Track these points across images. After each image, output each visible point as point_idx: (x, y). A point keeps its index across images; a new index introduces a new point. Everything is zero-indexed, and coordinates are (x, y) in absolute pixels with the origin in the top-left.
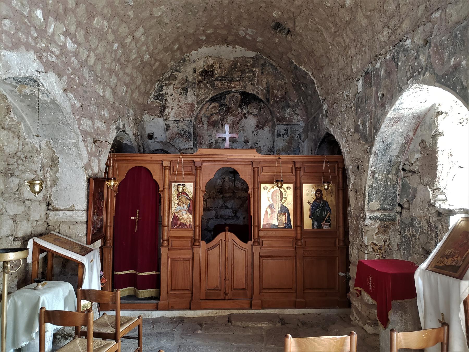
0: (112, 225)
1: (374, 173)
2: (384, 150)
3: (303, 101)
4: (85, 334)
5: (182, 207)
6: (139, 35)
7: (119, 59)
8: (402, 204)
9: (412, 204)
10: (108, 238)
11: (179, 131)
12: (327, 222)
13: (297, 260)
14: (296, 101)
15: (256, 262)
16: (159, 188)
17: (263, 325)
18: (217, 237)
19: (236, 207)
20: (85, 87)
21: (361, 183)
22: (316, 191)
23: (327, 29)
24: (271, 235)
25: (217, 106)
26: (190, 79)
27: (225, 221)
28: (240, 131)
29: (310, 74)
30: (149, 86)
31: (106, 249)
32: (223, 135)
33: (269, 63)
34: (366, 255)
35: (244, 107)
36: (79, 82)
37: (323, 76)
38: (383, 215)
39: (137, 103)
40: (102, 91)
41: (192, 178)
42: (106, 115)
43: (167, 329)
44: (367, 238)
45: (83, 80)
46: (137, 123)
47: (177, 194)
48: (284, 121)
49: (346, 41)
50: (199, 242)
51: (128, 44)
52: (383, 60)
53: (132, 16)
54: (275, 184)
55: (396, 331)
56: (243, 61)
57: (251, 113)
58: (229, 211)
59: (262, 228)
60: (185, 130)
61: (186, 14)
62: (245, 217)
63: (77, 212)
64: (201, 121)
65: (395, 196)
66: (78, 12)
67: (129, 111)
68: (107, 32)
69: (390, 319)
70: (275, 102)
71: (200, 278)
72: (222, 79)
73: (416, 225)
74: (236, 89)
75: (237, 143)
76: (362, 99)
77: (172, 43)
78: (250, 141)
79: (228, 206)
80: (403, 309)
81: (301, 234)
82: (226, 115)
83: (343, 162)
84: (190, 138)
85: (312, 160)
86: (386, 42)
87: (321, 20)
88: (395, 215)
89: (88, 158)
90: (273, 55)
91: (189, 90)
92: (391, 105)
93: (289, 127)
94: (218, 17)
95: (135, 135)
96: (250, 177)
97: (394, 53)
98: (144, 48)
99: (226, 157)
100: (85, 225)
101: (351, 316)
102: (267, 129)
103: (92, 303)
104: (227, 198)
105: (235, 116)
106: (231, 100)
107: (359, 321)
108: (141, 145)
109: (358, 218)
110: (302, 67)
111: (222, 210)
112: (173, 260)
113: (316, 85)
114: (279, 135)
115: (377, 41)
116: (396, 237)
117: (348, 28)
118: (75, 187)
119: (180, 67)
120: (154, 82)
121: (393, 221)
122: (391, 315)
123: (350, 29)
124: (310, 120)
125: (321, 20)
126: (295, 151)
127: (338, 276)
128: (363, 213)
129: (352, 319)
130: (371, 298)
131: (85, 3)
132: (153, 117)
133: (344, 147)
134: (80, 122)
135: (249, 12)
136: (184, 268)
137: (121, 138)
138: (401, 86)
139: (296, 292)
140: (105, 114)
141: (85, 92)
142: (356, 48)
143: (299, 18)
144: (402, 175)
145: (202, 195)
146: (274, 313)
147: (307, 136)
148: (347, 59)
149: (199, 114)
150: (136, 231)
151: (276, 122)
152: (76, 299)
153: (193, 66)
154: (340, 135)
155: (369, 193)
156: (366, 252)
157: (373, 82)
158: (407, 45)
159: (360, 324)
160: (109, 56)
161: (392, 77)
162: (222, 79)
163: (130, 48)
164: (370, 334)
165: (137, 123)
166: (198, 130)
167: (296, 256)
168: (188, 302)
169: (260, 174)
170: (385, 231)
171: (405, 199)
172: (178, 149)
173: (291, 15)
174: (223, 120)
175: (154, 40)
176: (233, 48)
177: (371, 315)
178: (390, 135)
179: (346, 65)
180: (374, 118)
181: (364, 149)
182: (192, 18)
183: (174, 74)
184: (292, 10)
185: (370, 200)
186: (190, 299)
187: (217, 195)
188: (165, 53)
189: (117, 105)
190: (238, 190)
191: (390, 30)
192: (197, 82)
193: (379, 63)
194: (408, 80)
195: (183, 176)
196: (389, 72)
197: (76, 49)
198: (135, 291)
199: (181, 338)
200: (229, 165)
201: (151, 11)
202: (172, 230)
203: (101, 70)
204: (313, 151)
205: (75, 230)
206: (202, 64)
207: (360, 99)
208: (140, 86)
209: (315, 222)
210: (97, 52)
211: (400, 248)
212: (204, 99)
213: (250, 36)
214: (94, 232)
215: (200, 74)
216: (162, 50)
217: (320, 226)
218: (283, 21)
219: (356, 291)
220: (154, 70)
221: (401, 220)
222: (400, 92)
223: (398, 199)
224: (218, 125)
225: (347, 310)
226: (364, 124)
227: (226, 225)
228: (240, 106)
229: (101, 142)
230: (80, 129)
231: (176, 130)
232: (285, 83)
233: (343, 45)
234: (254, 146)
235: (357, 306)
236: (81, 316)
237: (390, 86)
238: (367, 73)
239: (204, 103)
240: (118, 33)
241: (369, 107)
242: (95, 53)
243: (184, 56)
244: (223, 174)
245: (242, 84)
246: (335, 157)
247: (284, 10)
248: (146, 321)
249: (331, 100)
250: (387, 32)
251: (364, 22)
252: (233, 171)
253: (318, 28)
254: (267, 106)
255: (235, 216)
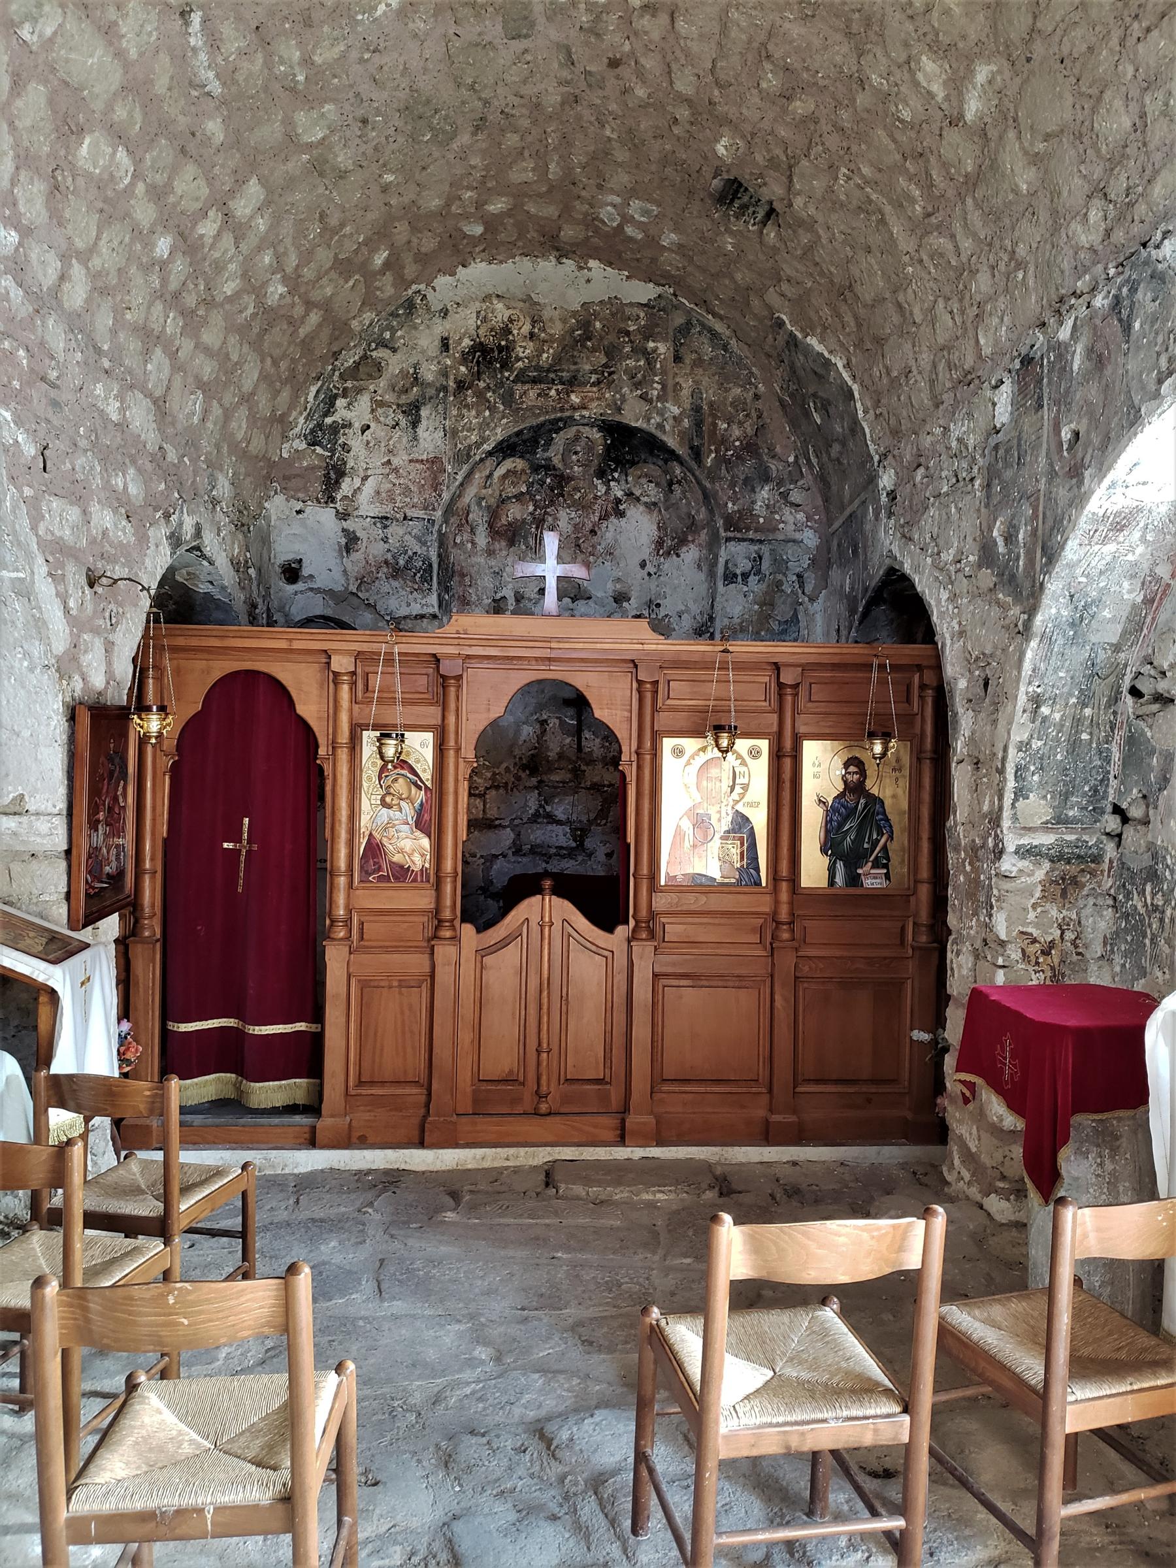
0: (159, 868)
1: (1037, 701)
2: (1073, 625)
3: (814, 460)
4: (55, 1219)
5: (398, 813)
6: (248, 211)
7: (177, 295)
8: (1124, 806)
9: (1156, 808)
10: (147, 910)
11: (389, 556)
12: (876, 865)
13: (777, 988)
14: (791, 459)
15: (642, 992)
16: (317, 746)
17: (659, 1196)
18: (513, 913)
19: (584, 819)
20: (53, 386)
21: (993, 735)
22: (846, 765)
23: (901, 205)
24: (693, 908)
25: (523, 470)
26: (429, 373)
27: (544, 865)
28: (601, 560)
29: (840, 365)
30: (285, 395)
31: (139, 946)
32: (538, 569)
33: (703, 325)
34: (1001, 972)
35: (616, 475)
36: (32, 370)
37: (884, 371)
38: (1061, 843)
39: (244, 455)
40: (118, 404)
41: (432, 714)
42: (133, 490)
43: (343, 1209)
44: (1004, 916)
45: (47, 361)
46: (243, 525)
47: (379, 767)
48: (748, 529)
49: (962, 250)
50: (453, 927)
51: (208, 241)
52: (1083, 312)
53: (219, 137)
54: (710, 740)
55: (1071, 1203)
56: (613, 315)
57: (638, 499)
58: (559, 829)
59: (663, 883)
60: (410, 553)
61: (413, 138)
62: (613, 852)
63: (33, 818)
64: (465, 522)
65: (1104, 781)
66: (19, 110)
67: (216, 480)
68: (129, 191)
69: (1063, 1172)
70: (721, 460)
71: (455, 1044)
72: (538, 377)
73: (1167, 873)
74: (586, 413)
75: (591, 602)
76: (1007, 451)
77: (366, 243)
78: (634, 595)
79: (556, 813)
80: (1107, 1140)
81: (791, 903)
82: (552, 503)
83: (938, 667)
84: (426, 577)
85: (836, 660)
86: (1095, 251)
87: (880, 170)
88: (1099, 841)
89: (68, 637)
90: (717, 298)
91: (424, 412)
92: (1103, 469)
93: (765, 549)
94: (526, 153)
95: (236, 565)
96: (627, 714)
97: (1120, 289)
98: (267, 260)
99: (548, 645)
100: (63, 865)
101: (945, 1169)
102: (691, 554)
103: (87, 1120)
104: (556, 788)
105: (583, 506)
106: (569, 450)
107: (969, 1183)
108: (260, 601)
109: (980, 853)
110: (812, 341)
111: (535, 826)
112: (364, 985)
113: (859, 405)
114: (730, 578)
115: (1066, 248)
116: (1102, 916)
117: (969, 201)
118: (26, 733)
119: (393, 331)
120: (305, 382)
121: (1093, 861)
122: (1068, 1159)
123: (978, 206)
124: (836, 525)
125: (880, 170)
126: (784, 632)
127: (908, 1040)
128: (996, 836)
129: (949, 1178)
130: (1009, 1106)
131: (46, 82)
132: (299, 506)
133: (942, 615)
134: (38, 509)
135: (631, 138)
136: (402, 1013)
137: (189, 574)
138: (1136, 402)
139: (770, 1091)
140: (130, 486)
141: (55, 404)
142: (996, 273)
143: (804, 163)
144: (1131, 710)
145: (465, 771)
146: (697, 1157)
147: (824, 582)
148: (962, 312)
149: (459, 496)
150: (240, 890)
151: (721, 531)
152: (31, 1103)
153: (440, 328)
154: (931, 574)
155: (1018, 769)
156: (1000, 962)
157: (1046, 391)
158: (1165, 259)
159: (974, 1192)
160: (140, 281)
161: (1108, 371)
162: (538, 377)
163: (217, 255)
164: (1003, 1224)
165: (243, 525)
166: (455, 555)
167: (772, 976)
168: (416, 1121)
169: (660, 704)
170: (1064, 893)
171: (1135, 791)
172: (388, 618)
173: (778, 151)
174: (544, 520)
175: (300, 231)
176: (581, 268)
177: (1007, 1161)
178: (1095, 572)
179: (959, 333)
180: (1044, 514)
181: (1007, 621)
182: (436, 154)
183: (374, 354)
184: (783, 133)
185: (1020, 793)
186: (422, 1111)
187: (519, 779)
188: (341, 282)
189: (172, 456)
190: (591, 762)
191: (1111, 206)
192: (451, 384)
193: (1070, 323)
194: (1160, 382)
195: (399, 708)
196: (1100, 356)
197: (17, 249)
198: (237, 1087)
199: (386, 1237)
200: (557, 673)
201: (288, 122)
202: (364, 888)
203: (114, 332)
204: (844, 632)
205: (28, 880)
206: (472, 322)
207: (1001, 452)
208: (253, 394)
209: (840, 865)
210: (96, 263)
211: (1112, 951)
212: (478, 445)
213: (639, 225)
214: (94, 888)
215: (465, 358)
216: (331, 268)
217: (853, 880)
218: (752, 174)
219: (961, 1087)
220: (303, 341)
221: (1120, 859)
222: (1132, 424)
223: (1111, 791)
224: (525, 538)
225: (934, 1150)
226: (1009, 538)
227: (546, 874)
228: (601, 474)
229: (116, 581)
230: (37, 535)
231: (378, 550)
232: (756, 395)
233: (954, 263)
234: (646, 613)
235: (966, 1135)
236: (41, 1156)
237: (1101, 404)
238: (1027, 361)
239: (477, 458)
240: (172, 199)
241: (1030, 478)
242: (87, 268)
243: (410, 292)
244: (540, 707)
245: (607, 395)
246: (914, 651)
247: (753, 135)
248: (275, 1183)
249: (908, 457)
250: (1101, 214)
251: (1026, 178)
252: (573, 695)
253: (870, 201)
254: (693, 475)
255: (579, 848)
